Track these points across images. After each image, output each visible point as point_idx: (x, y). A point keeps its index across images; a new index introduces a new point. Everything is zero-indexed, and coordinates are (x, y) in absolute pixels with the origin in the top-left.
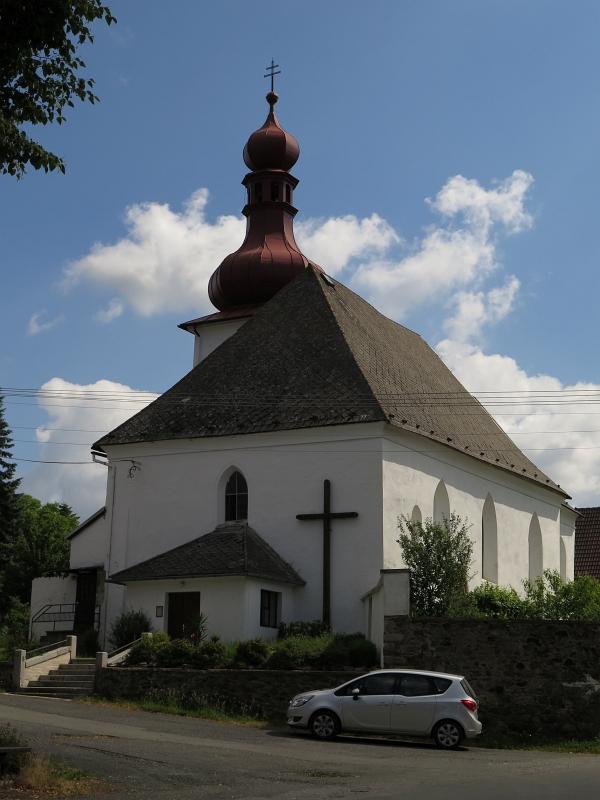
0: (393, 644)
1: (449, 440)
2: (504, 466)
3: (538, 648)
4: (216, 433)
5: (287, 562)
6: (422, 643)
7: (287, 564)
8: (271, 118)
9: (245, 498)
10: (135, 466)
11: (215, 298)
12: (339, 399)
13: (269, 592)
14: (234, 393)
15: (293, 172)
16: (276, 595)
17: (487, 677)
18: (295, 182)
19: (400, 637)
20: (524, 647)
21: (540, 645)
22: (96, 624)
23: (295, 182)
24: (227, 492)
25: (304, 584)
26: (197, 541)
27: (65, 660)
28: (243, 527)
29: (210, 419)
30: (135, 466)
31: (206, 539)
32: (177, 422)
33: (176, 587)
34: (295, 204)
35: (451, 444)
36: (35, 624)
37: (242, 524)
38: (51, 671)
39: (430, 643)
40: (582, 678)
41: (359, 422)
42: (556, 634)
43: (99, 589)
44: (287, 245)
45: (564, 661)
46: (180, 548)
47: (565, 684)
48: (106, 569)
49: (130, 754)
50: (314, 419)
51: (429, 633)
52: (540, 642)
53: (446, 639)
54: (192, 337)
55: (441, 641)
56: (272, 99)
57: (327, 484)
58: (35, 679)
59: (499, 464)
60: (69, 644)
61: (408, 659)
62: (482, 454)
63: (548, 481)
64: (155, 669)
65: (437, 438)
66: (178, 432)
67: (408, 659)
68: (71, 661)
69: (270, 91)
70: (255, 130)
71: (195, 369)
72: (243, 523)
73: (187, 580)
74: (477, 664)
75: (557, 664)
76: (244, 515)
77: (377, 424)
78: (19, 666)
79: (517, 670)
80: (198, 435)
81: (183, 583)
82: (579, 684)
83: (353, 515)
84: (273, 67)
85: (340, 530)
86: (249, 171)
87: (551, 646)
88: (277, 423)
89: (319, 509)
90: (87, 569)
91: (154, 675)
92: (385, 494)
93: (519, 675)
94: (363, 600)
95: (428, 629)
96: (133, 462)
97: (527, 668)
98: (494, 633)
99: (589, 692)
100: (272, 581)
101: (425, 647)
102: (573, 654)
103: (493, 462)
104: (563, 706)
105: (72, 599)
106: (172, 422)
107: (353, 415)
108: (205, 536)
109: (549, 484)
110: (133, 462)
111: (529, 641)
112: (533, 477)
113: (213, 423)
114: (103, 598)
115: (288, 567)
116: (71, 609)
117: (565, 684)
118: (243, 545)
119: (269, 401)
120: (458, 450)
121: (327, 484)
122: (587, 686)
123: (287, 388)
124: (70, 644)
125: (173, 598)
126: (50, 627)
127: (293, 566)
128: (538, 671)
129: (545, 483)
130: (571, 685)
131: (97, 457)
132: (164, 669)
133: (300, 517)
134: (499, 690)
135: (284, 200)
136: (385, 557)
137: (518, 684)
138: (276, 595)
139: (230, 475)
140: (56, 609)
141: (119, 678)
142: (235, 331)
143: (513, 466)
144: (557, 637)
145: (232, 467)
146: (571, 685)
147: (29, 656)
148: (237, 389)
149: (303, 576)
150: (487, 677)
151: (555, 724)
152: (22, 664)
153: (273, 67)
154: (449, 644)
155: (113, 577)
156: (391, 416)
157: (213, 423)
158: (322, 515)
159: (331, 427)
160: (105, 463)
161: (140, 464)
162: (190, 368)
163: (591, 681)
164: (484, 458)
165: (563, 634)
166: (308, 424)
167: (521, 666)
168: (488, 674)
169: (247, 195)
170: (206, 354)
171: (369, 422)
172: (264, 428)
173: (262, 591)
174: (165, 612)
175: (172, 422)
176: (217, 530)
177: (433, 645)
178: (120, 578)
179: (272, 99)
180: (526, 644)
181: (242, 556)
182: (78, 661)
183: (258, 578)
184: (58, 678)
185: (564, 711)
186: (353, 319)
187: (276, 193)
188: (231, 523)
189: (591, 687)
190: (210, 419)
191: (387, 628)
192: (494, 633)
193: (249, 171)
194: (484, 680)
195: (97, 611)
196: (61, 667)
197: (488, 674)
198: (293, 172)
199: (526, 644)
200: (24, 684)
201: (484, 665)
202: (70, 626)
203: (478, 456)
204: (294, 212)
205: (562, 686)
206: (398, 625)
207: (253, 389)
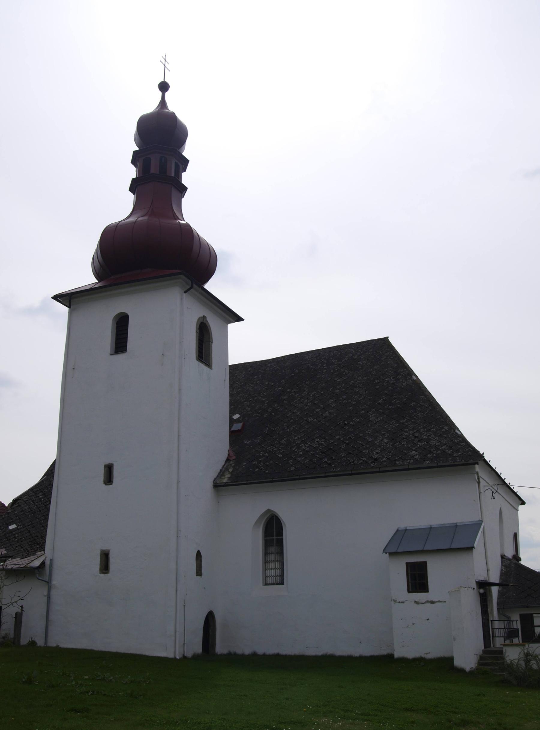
8: (163, 103)
56: (164, 87)
86: (137, 149)
121: (199, 555)
127: (296, 654)
135: (173, 175)
160: (513, 623)
179: (164, 87)
193: (137, 149)
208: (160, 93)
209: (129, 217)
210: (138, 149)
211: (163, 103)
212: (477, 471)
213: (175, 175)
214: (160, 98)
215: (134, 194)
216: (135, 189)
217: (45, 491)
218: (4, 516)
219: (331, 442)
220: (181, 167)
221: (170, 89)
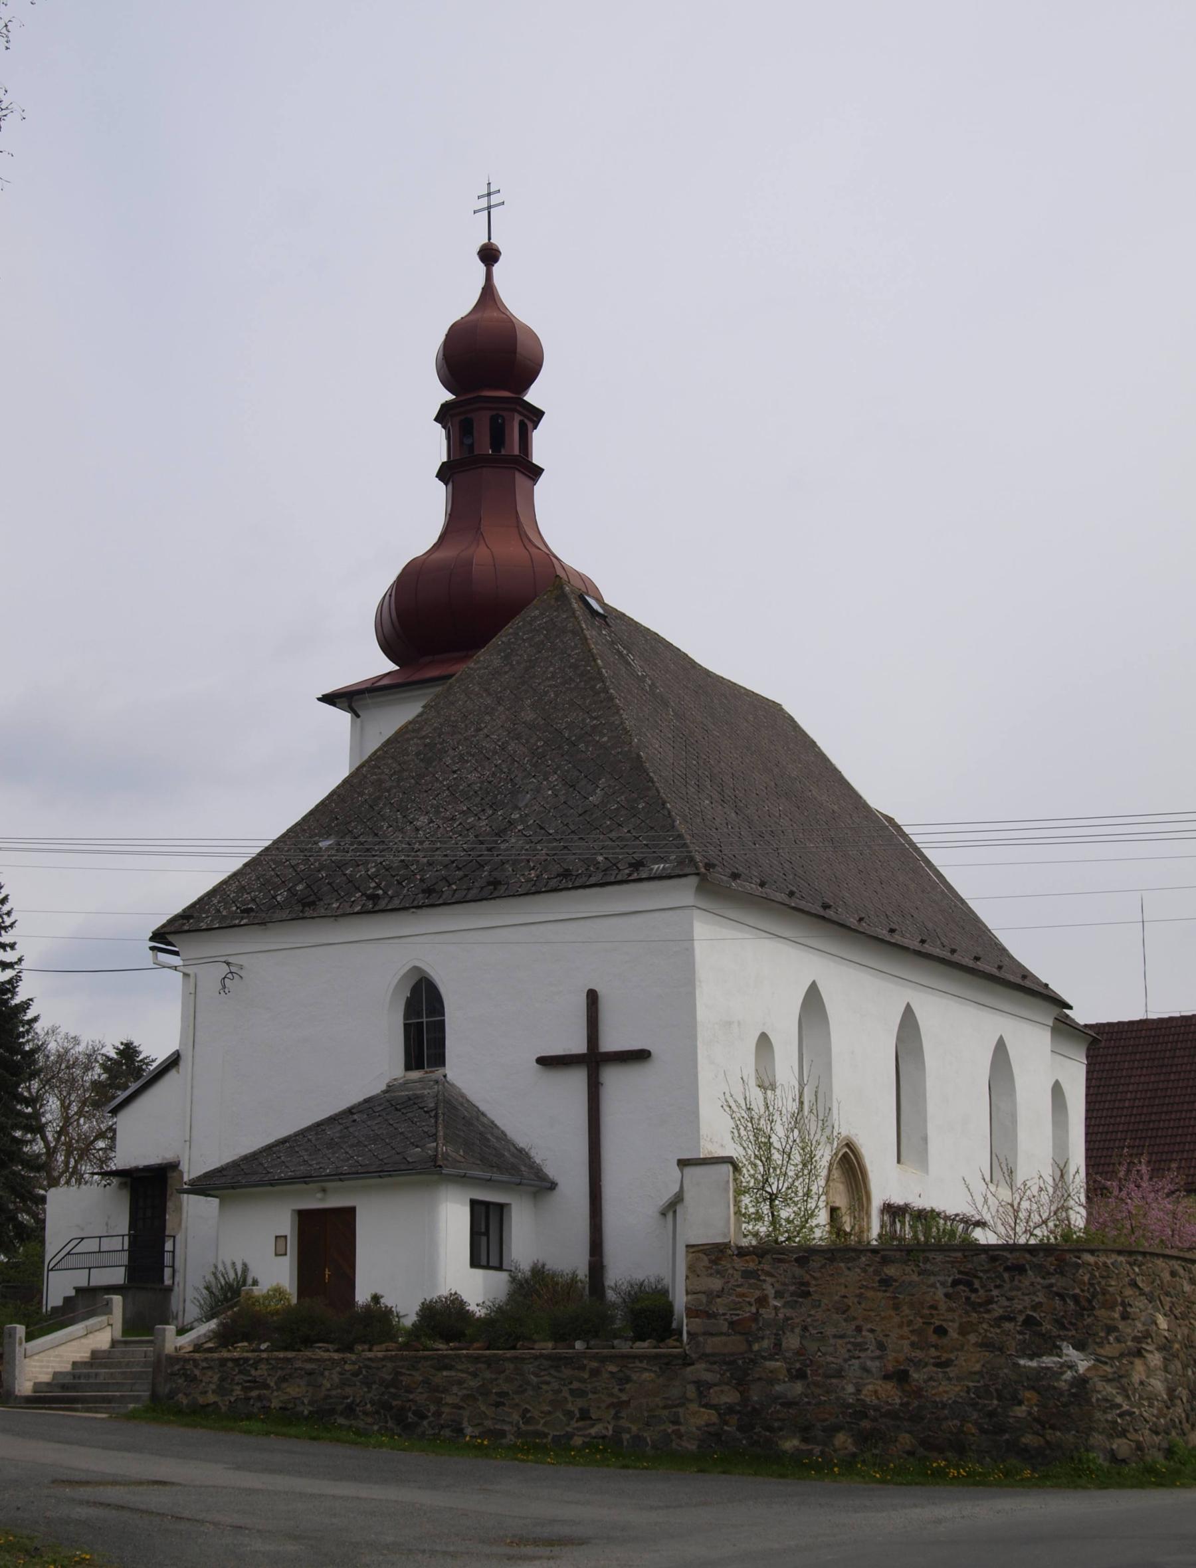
0: (704, 1298)
1: (826, 907)
2: (937, 951)
3: (973, 1296)
4: (382, 904)
5: (521, 1145)
6: (758, 1293)
7: (521, 1151)
8: (489, 293)
9: (440, 1027)
10: (233, 972)
11: (389, 647)
12: (613, 835)
13: (487, 1204)
14: (417, 830)
15: (533, 396)
16: (501, 1209)
17: (878, 1353)
18: (536, 415)
19: (716, 1284)
20: (947, 1295)
21: (976, 1291)
22: (167, 1272)
23: (536, 415)
24: (407, 1015)
25: (553, 1186)
26: (350, 1111)
27: (102, 1339)
28: (437, 1082)
29: (371, 878)
30: (233, 972)
31: (367, 1106)
32: (308, 886)
33: (314, 1202)
34: (537, 459)
35: (830, 913)
36: (50, 1273)
37: (434, 1076)
38: (74, 1363)
39: (771, 1292)
40: (1056, 1350)
41: (650, 879)
42: (1007, 1269)
43: (170, 1204)
44: (523, 538)
45: (1021, 1318)
46: (318, 1125)
47: (1022, 1362)
48: (184, 1167)
49: (186, 1514)
50: (566, 874)
51: (772, 1275)
52: (977, 1284)
53: (802, 1284)
54: (347, 717)
55: (792, 1288)
56: (489, 255)
57: (593, 998)
58: (45, 1378)
59: (927, 948)
60: (107, 1309)
61: (732, 1324)
62: (892, 931)
63: (1024, 977)
64: (264, 1355)
65: (802, 904)
66: (312, 904)
67: (732, 1324)
68: (114, 1343)
69: (487, 241)
70: (457, 318)
71: (352, 775)
72: (438, 1073)
73: (328, 1185)
74: (859, 1329)
75: (1008, 1326)
76: (439, 1059)
77: (683, 880)
78: (14, 1358)
79: (933, 1339)
80: (349, 910)
81: (324, 1190)
82: (1048, 1361)
83: (641, 1056)
84: (489, 194)
85: (614, 1080)
86: (449, 396)
87: (995, 1293)
88: (496, 883)
89: (577, 1045)
90: (148, 1169)
91: (263, 1366)
92: (702, 1014)
93: (936, 1347)
94: (664, 1214)
95: (767, 1267)
96: (228, 964)
97: (953, 1334)
98: (891, 1271)
99: (1069, 1375)
100: (488, 1183)
101: (762, 1301)
102: (1036, 1307)
103: (915, 945)
104: (1020, 1403)
105: (122, 1225)
106: (300, 887)
107: (637, 865)
108: (366, 1101)
109: (1027, 983)
110: (228, 964)
111: (955, 1283)
112: (995, 971)
113: (378, 886)
114: (180, 1225)
115: (522, 1155)
116: (119, 1244)
117: (1022, 1362)
118: (436, 1116)
119: (482, 843)
120: (842, 925)
121: (593, 998)
122: (1062, 1365)
123: (516, 816)
124: (110, 1312)
125: (305, 1218)
126: (80, 1279)
127: (533, 1153)
128: (972, 1338)
129: (1019, 981)
130: (1034, 1364)
131: (163, 957)
132: (281, 1355)
133: (544, 1061)
134: (901, 1377)
135: (516, 452)
136: (704, 1131)
137: (937, 1365)
138: (501, 1208)
139: (413, 983)
140: (91, 1245)
141: (197, 1372)
142: (420, 710)
143: (953, 951)
144: (1006, 1276)
145: (416, 969)
146: (1034, 1364)
147: (30, 1337)
148: (423, 820)
149: (551, 1171)
150: (878, 1353)
151: (1007, 1436)
152: (19, 1351)
153: (489, 194)
154: (808, 1294)
155: (192, 1183)
156: (709, 866)
157: (378, 886)
158: (583, 1055)
159: (581, 891)
160: (175, 968)
161: (241, 967)
162: (345, 773)
163: (1071, 1353)
164: (896, 938)
165: (1020, 1269)
166: (553, 883)
167: (941, 1331)
168: (881, 1346)
169: (445, 442)
170: (373, 744)
171: (670, 877)
172: (396, 903)
173: (474, 1203)
174: (292, 1246)
175: (300, 887)
176: (390, 1088)
177: (779, 1295)
178: (206, 1185)
179: (489, 255)
180: (950, 1290)
181: (434, 1137)
182: (126, 1343)
183: (463, 1180)
184: (88, 1376)
185: (1020, 1411)
186: (642, 679)
187: (498, 437)
188: (415, 1075)
189: (1072, 1366)
190: (371, 878)
191: (691, 1268)
192: (891, 1271)
193: (449, 396)
194: (873, 1359)
195: (168, 1246)
196: (95, 1354)
197: (881, 1346)
198: (533, 396)
199: (950, 1290)
200: (24, 1387)
201: (872, 1331)
202: (117, 1276)
203: (883, 933)
204: (536, 472)
205: (1016, 1365)
206: (711, 1261)
207: (453, 819)
208: (481, 268)
209: (436, 547)
210: (454, 397)
211: (489, 293)
212: (574, 1382)
213: (520, 452)
214: (481, 282)
215: (446, 484)
216: (449, 478)
217: (474, 1375)
218: (316, 1416)
219: (361, 1437)
220: (530, 425)
221: (501, 258)
